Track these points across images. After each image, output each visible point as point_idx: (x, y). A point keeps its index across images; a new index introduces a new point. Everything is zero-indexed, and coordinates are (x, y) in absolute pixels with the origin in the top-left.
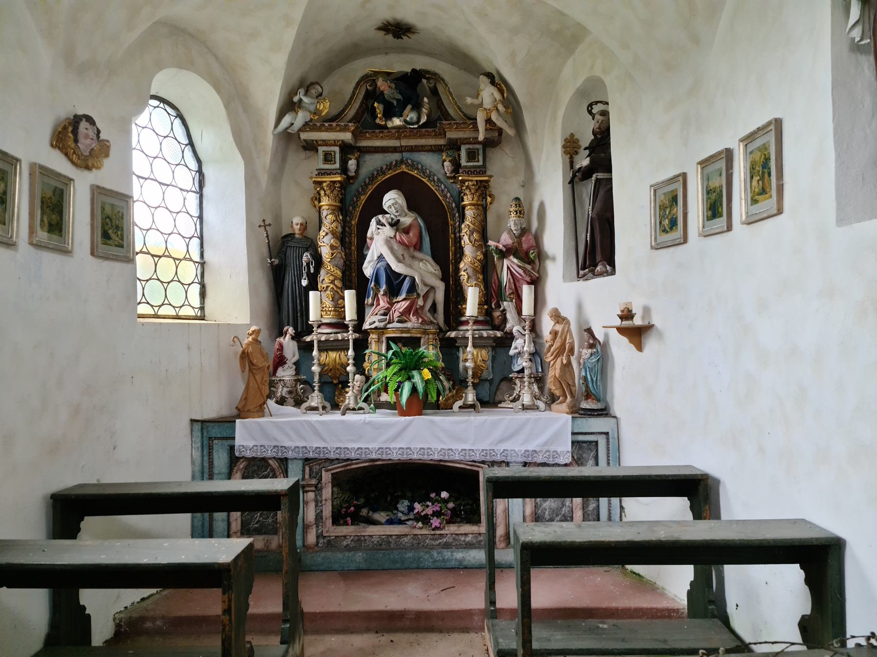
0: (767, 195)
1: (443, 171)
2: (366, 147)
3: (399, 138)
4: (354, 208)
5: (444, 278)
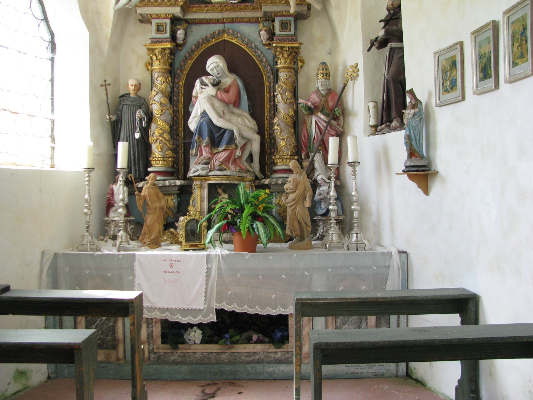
0: (525, 59)
1: (259, 39)
2: (191, 19)
3: (221, 11)
4: (182, 71)
5: (261, 131)
